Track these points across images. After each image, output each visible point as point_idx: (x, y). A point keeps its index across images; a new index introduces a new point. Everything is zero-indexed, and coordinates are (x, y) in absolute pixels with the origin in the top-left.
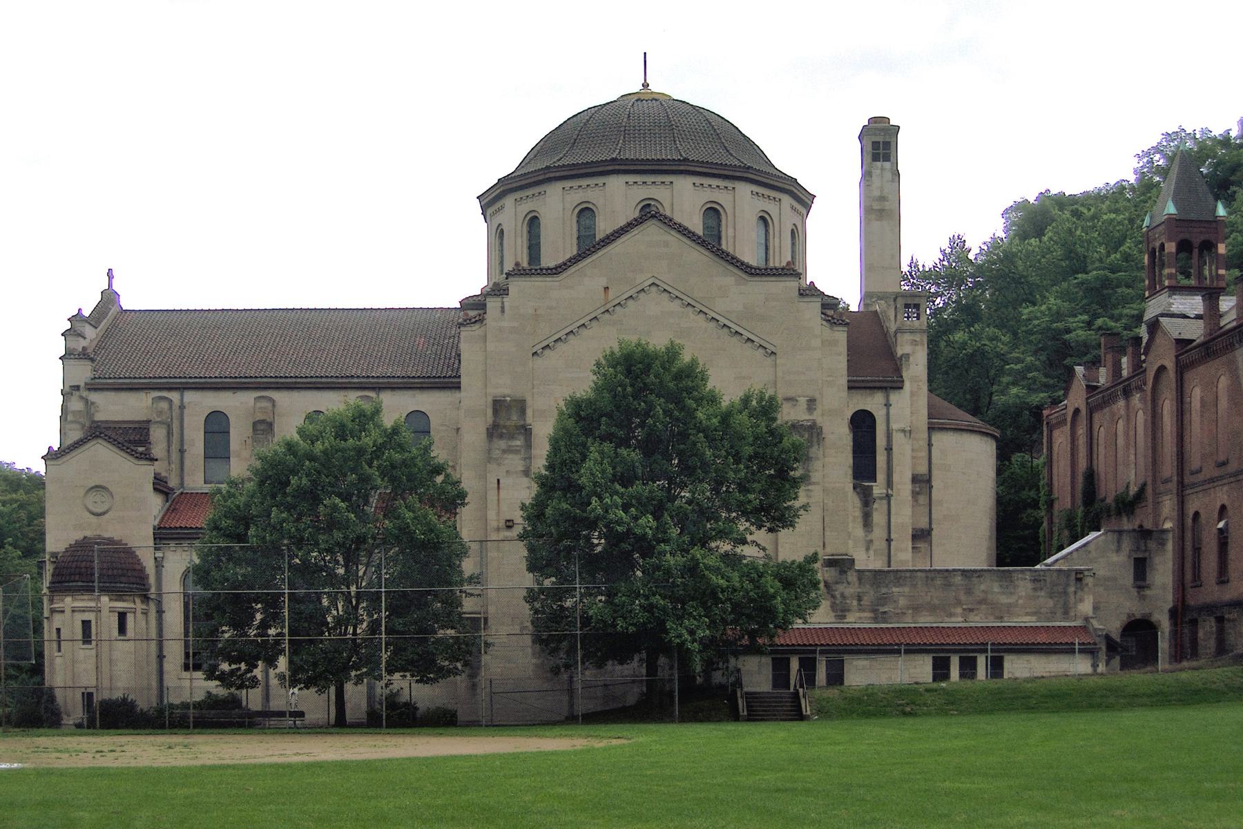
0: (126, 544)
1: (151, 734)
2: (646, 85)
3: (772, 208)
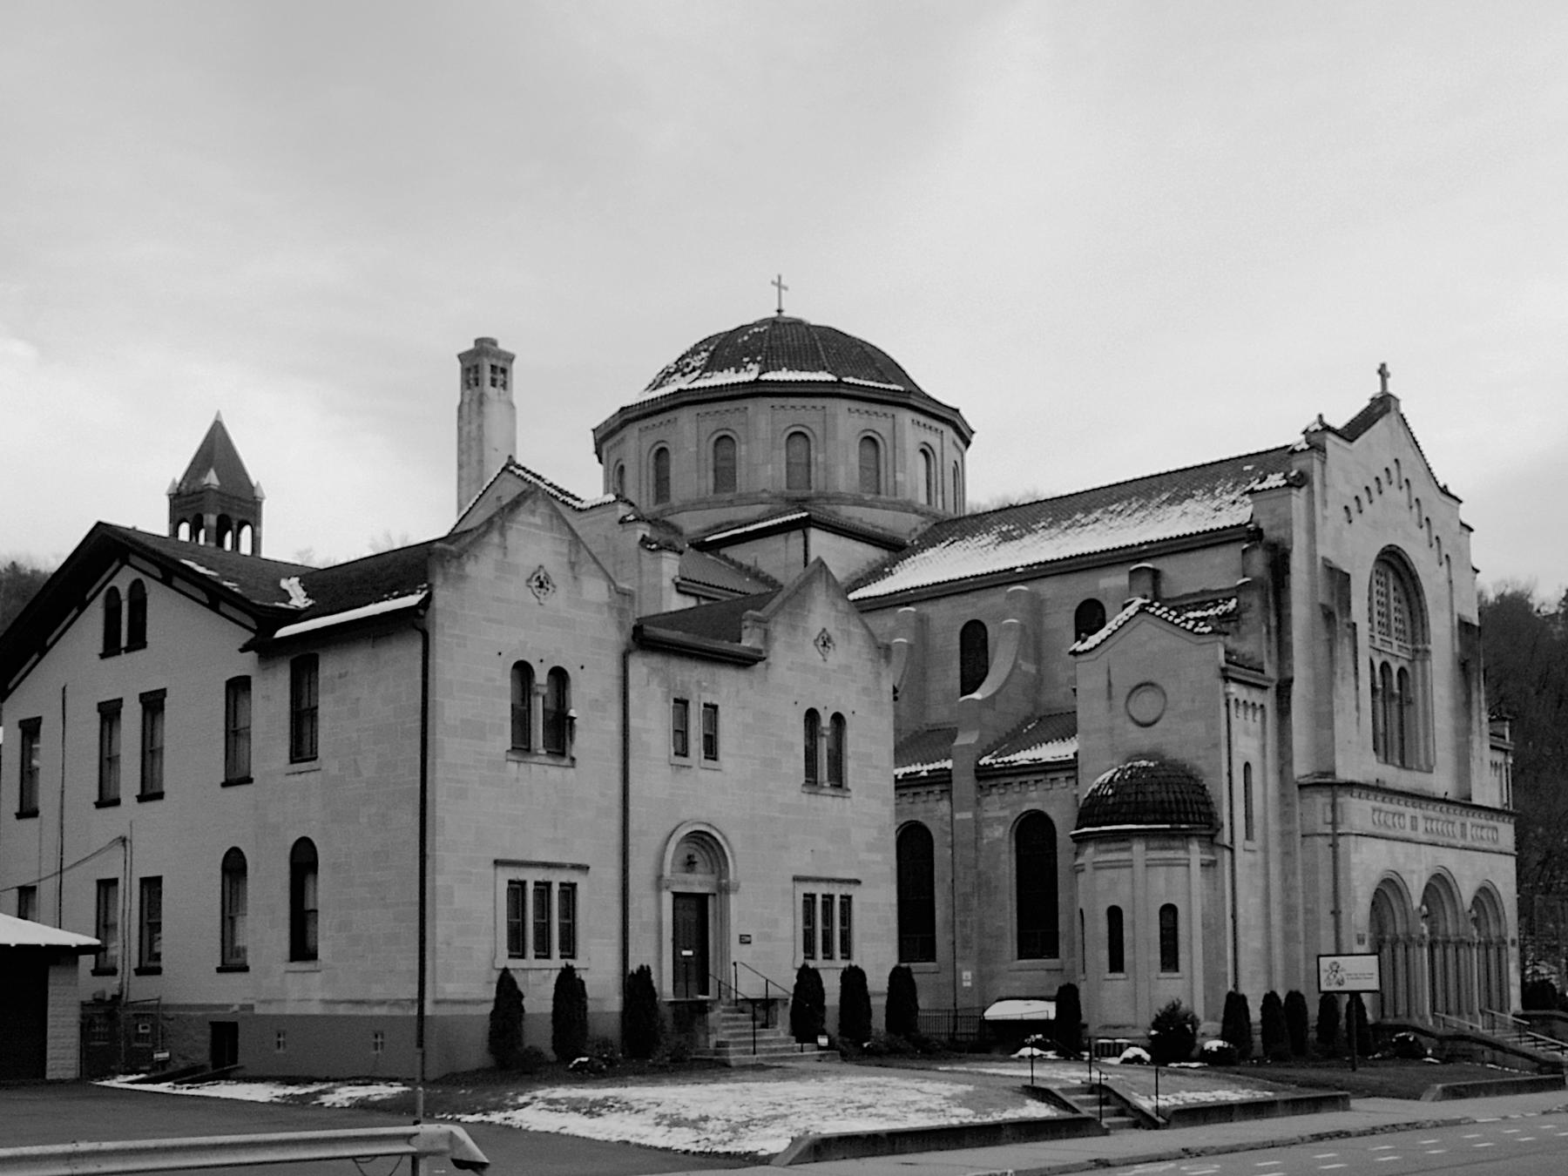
0: (1040, 759)
3: (934, 440)
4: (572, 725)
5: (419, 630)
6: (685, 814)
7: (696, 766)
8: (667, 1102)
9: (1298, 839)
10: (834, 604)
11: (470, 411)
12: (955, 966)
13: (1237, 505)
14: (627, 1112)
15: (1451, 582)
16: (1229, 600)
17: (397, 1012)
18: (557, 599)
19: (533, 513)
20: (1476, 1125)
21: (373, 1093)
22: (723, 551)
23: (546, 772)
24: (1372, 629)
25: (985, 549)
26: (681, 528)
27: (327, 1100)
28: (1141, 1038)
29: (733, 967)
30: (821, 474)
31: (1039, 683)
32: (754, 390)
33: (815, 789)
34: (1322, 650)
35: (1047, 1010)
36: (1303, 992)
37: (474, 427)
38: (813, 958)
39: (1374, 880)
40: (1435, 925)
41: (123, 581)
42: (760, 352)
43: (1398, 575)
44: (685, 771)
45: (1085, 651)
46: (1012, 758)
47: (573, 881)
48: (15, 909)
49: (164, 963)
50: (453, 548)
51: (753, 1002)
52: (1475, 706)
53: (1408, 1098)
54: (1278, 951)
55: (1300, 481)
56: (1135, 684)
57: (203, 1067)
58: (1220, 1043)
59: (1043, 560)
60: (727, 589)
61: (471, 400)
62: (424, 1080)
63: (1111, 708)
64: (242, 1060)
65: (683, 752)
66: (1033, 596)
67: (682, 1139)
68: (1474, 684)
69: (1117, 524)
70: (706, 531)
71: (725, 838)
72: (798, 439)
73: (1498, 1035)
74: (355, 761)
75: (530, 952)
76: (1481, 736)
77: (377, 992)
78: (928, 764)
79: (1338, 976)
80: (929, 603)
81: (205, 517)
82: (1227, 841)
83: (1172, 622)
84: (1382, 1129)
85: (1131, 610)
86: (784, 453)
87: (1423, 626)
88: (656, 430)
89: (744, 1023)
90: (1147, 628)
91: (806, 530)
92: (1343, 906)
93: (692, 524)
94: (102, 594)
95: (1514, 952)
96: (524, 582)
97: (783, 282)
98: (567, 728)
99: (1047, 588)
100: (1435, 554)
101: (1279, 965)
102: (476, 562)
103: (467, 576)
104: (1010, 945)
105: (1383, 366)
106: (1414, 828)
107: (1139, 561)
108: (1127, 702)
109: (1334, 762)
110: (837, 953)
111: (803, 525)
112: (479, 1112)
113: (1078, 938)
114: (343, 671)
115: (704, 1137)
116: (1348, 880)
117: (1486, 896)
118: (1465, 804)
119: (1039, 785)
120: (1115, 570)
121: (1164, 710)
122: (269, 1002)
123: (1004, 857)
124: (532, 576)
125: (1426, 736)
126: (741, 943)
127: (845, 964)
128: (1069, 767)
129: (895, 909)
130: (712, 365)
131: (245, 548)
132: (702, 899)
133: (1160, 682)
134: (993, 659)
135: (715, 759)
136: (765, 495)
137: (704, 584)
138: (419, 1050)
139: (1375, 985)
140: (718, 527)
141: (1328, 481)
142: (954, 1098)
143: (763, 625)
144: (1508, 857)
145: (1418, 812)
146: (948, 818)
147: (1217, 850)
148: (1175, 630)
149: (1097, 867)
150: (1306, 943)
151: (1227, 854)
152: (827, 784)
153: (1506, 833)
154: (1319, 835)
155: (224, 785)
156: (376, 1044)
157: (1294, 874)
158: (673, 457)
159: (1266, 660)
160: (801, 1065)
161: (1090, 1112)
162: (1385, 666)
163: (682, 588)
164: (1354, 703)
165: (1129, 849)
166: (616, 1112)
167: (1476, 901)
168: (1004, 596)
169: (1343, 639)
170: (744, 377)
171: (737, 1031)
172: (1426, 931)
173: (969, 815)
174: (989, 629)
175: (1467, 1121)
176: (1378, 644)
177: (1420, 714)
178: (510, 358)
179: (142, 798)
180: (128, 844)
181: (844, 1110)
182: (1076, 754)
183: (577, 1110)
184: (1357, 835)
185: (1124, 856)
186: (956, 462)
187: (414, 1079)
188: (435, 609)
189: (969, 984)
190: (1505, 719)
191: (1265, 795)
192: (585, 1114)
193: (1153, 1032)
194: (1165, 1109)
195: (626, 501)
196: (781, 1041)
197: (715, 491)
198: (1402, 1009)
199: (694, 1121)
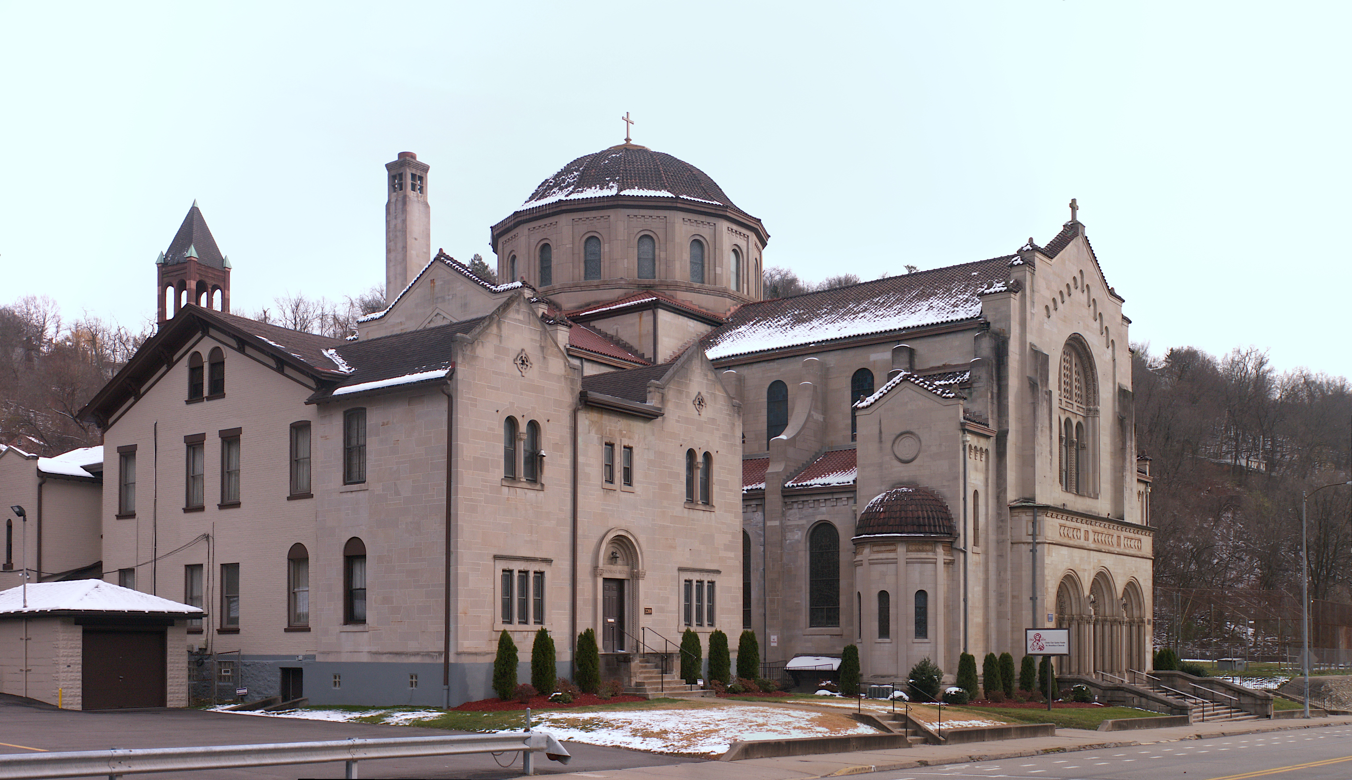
0: (829, 484)
1: (959, 710)
2: (628, 140)
3: (742, 243)
4: (541, 460)
5: (446, 394)
6: (611, 524)
7: (618, 490)
8: (634, 721)
9: (1009, 545)
10: (706, 375)
11: (396, 209)
12: (765, 631)
13: (969, 304)
14: (610, 728)
15: (1114, 360)
16: (965, 373)
17: (428, 660)
18: (532, 373)
19: (518, 311)
20: (1140, 747)
21: (421, 716)
22: (592, 324)
23: (526, 494)
24: (1060, 395)
25: (784, 328)
26: (561, 306)
27: (388, 720)
28: (902, 684)
29: (641, 631)
30: (663, 267)
31: (825, 428)
32: (616, 203)
33: (692, 506)
34: (1028, 410)
35: (835, 664)
36: (1010, 654)
37: (399, 221)
38: (690, 625)
39: (1060, 575)
40: (1098, 608)
41: (205, 347)
42: (618, 173)
43: (1079, 356)
44: (611, 493)
45: (863, 408)
46: (809, 483)
47: (542, 570)
48: (118, 581)
49: (241, 626)
50: (468, 336)
51: (655, 655)
52: (1128, 450)
53: (1090, 729)
54: (993, 625)
55: (1017, 287)
56: (898, 432)
57: (275, 700)
58: (957, 689)
59: (829, 338)
60: (601, 354)
61: (397, 200)
62: (449, 707)
63: (881, 449)
64: (306, 693)
65: (611, 480)
66: (822, 364)
67: (655, 745)
68: (1128, 435)
69: (881, 313)
70: (580, 307)
71: (636, 540)
72: (647, 241)
73: (1139, 687)
74: (395, 484)
75: (516, 619)
76: (1131, 473)
77: (413, 646)
78: (747, 486)
79: (1040, 643)
80: (745, 367)
81: (187, 282)
82: (962, 547)
83: (926, 389)
84: (1084, 748)
85: (897, 379)
86: (636, 251)
87: (1094, 392)
88: (541, 230)
89: (652, 670)
90: (908, 392)
91: (656, 310)
92: (1038, 594)
93: (569, 302)
94: (187, 357)
95: (1149, 628)
96: (512, 361)
97: (631, 118)
98: (539, 463)
99: (832, 359)
100: (1105, 339)
101: (993, 636)
102: (483, 346)
103: (477, 357)
104: (804, 617)
105: (1074, 201)
106: (1087, 539)
107: (899, 342)
108: (892, 446)
109: (1035, 491)
110: (706, 622)
111: (653, 306)
112: (507, 728)
113: (856, 612)
114: (385, 421)
115: (670, 744)
116: (1043, 576)
117: (1132, 587)
118: (1118, 521)
119: (828, 502)
120: (881, 348)
121: (919, 451)
122: (328, 653)
123: (802, 553)
124: (518, 356)
125: (1094, 472)
126: (645, 614)
127: (539, 627)
128: (850, 490)
129: (742, 591)
130: (583, 183)
131: (217, 305)
132: (620, 582)
133: (916, 432)
134: (793, 409)
135: (630, 485)
136: (623, 282)
137: (586, 349)
138: (446, 687)
139: (1064, 650)
140: (588, 305)
141: (1035, 287)
142: (812, 720)
143: (661, 390)
144: (1148, 560)
145: (1089, 528)
146: (761, 525)
147: (955, 552)
148: (929, 395)
149: (872, 563)
150: (1013, 619)
151: (962, 555)
152: (700, 503)
153: (1147, 543)
154: (1024, 543)
155: (289, 499)
156: (335, 682)
157: (1006, 570)
158: (554, 251)
159: (990, 417)
160: (694, 698)
161: (900, 732)
162: (1068, 421)
163: (571, 353)
164: (1048, 449)
165: (894, 551)
166: (602, 728)
167: (1126, 591)
168: (801, 364)
169: (1042, 402)
170: (606, 193)
171: (647, 675)
172: (1092, 613)
173: (777, 523)
174: (789, 387)
175: (1135, 744)
176: (1063, 406)
177: (1091, 457)
178: (426, 169)
179: (222, 506)
180: (211, 539)
181: (750, 726)
182: (854, 481)
183: (575, 727)
184: (1049, 543)
185: (891, 555)
186: (756, 259)
187: (441, 707)
188: (457, 380)
189: (775, 645)
190: (1147, 460)
191: (987, 514)
192: (581, 729)
193: (911, 681)
194: (944, 731)
195: (530, 287)
196: (676, 682)
197: (586, 278)
198: (1074, 668)
199: (657, 733)
